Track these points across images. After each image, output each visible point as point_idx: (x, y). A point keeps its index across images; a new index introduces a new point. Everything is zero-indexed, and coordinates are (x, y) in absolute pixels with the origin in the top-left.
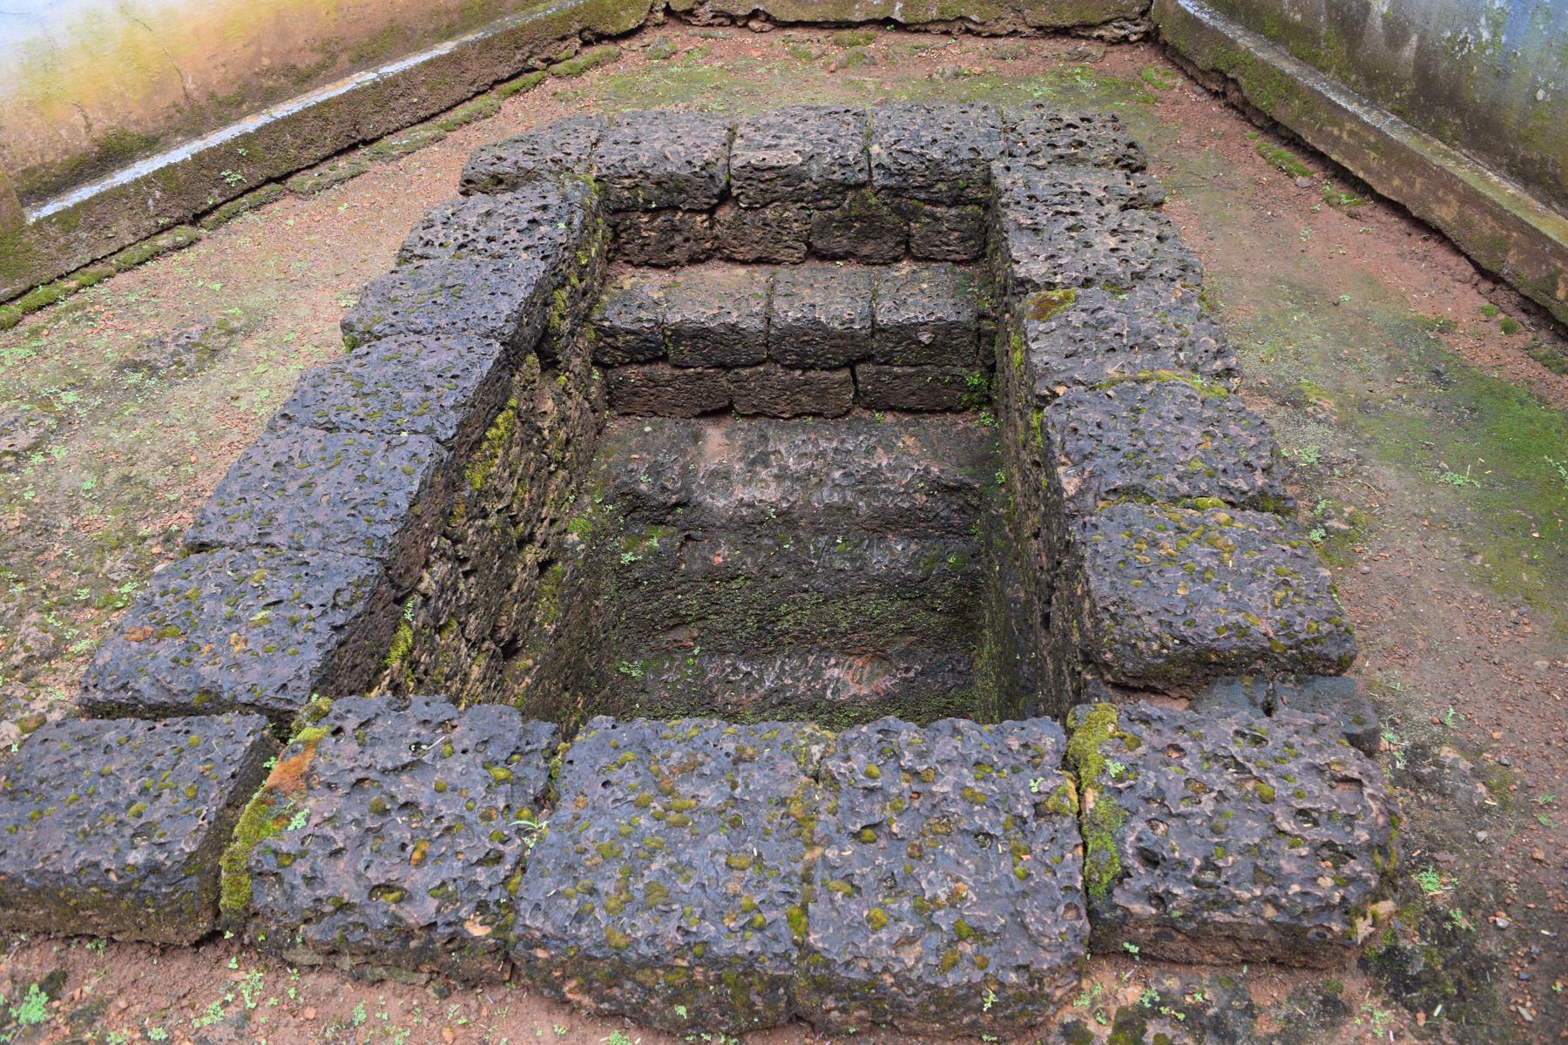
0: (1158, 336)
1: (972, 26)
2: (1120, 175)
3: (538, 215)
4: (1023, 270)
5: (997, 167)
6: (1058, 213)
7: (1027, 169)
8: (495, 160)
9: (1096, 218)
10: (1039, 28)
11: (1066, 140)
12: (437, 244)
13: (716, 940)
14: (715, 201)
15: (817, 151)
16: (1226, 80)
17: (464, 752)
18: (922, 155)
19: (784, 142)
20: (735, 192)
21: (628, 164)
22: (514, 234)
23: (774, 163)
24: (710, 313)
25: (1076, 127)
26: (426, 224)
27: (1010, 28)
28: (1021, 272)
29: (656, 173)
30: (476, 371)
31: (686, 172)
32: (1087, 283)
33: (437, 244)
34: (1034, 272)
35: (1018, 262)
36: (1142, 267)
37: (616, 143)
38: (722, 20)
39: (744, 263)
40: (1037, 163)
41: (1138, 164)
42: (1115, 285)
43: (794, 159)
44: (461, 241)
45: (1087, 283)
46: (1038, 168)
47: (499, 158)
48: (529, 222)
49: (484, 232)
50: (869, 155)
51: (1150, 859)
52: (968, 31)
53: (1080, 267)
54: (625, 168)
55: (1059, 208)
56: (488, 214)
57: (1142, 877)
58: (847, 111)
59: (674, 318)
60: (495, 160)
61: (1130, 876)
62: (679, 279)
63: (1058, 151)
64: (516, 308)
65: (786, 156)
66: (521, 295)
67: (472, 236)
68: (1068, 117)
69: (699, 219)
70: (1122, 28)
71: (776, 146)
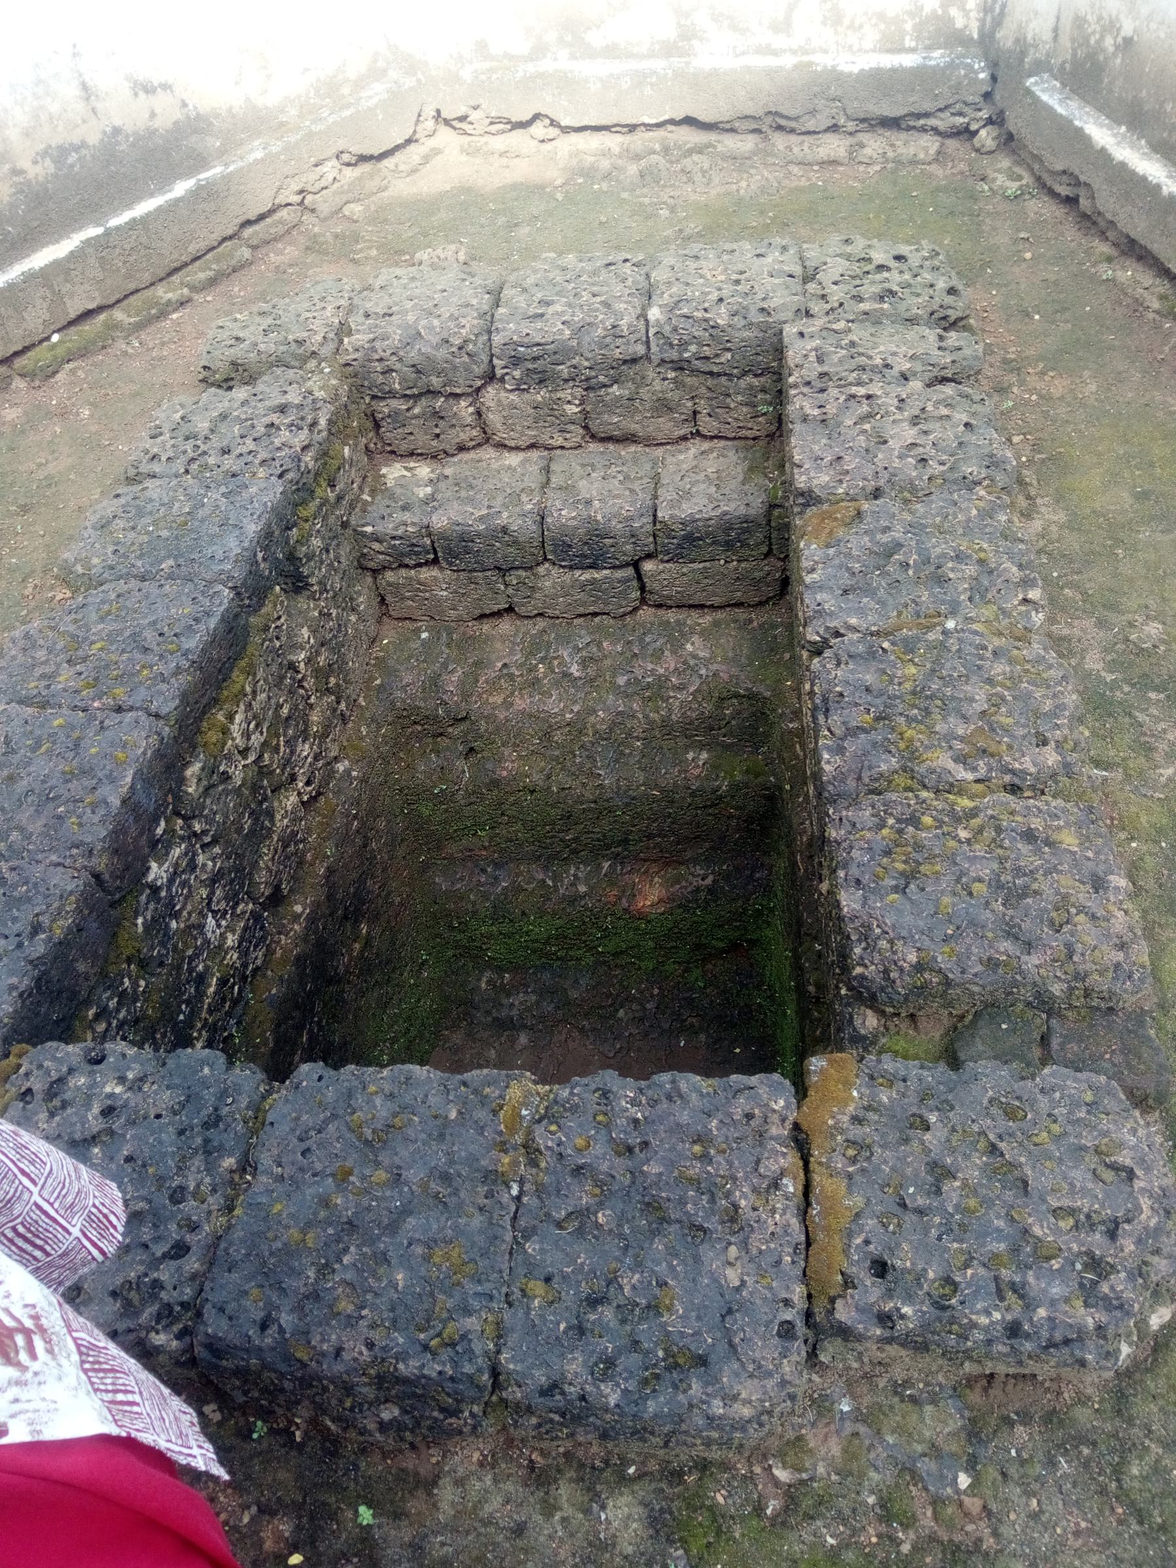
0: (950, 565)
1: (783, 122)
2: (932, 335)
3: (275, 418)
4: (804, 478)
5: (790, 331)
6: (853, 396)
7: (825, 333)
8: (232, 342)
9: (896, 402)
10: (863, 120)
11: (876, 289)
12: (164, 459)
13: (402, 1357)
14: (479, 383)
15: (588, 320)
16: (1078, 184)
17: (158, 1116)
18: (706, 320)
19: (551, 310)
20: (499, 372)
21: (377, 344)
22: (250, 444)
23: (538, 340)
24: (478, 514)
25: (889, 269)
26: (153, 432)
27: (830, 123)
28: (801, 481)
29: (413, 355)
30: (201, 626)
31: (442, 353)
32: (877, 494)
33: (164, 459)
34: (815, 482)
35: (800, 466)
36: (942, 468)
37: (367, 316)
38: (501, 126)
39: (517, 448)
40: (834, 326)
41: (960, 314)
42: (911, 494)
43: (561, 332)
44: (191, 454)
45: (877, 494)
46: (835, 332)
47: (237, 339)
48: (267, 426)
49: (216, 443)
50: (647, 320)
51: (881, 1268)
52: (780, 128)
53: (869, 473)
54: (375, 350)
55: (854, 390)
56: (224, 417)
57: (871, 1291)
58: (626, 261)
59: (439, 521)
60: (232, 342)
61: (855, 1287)
62: (448, 471)
63: (864, 306)
64: (246, 544)
65: (554, 330)
66: (252, 528)
67: (203, 447)
68: (879, 257)
69: (463, 404)
70: (960, 114)
71: (542, 315)
